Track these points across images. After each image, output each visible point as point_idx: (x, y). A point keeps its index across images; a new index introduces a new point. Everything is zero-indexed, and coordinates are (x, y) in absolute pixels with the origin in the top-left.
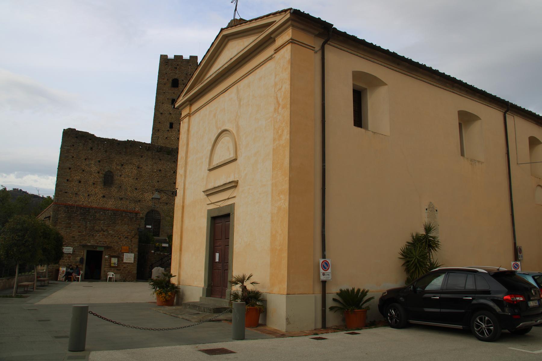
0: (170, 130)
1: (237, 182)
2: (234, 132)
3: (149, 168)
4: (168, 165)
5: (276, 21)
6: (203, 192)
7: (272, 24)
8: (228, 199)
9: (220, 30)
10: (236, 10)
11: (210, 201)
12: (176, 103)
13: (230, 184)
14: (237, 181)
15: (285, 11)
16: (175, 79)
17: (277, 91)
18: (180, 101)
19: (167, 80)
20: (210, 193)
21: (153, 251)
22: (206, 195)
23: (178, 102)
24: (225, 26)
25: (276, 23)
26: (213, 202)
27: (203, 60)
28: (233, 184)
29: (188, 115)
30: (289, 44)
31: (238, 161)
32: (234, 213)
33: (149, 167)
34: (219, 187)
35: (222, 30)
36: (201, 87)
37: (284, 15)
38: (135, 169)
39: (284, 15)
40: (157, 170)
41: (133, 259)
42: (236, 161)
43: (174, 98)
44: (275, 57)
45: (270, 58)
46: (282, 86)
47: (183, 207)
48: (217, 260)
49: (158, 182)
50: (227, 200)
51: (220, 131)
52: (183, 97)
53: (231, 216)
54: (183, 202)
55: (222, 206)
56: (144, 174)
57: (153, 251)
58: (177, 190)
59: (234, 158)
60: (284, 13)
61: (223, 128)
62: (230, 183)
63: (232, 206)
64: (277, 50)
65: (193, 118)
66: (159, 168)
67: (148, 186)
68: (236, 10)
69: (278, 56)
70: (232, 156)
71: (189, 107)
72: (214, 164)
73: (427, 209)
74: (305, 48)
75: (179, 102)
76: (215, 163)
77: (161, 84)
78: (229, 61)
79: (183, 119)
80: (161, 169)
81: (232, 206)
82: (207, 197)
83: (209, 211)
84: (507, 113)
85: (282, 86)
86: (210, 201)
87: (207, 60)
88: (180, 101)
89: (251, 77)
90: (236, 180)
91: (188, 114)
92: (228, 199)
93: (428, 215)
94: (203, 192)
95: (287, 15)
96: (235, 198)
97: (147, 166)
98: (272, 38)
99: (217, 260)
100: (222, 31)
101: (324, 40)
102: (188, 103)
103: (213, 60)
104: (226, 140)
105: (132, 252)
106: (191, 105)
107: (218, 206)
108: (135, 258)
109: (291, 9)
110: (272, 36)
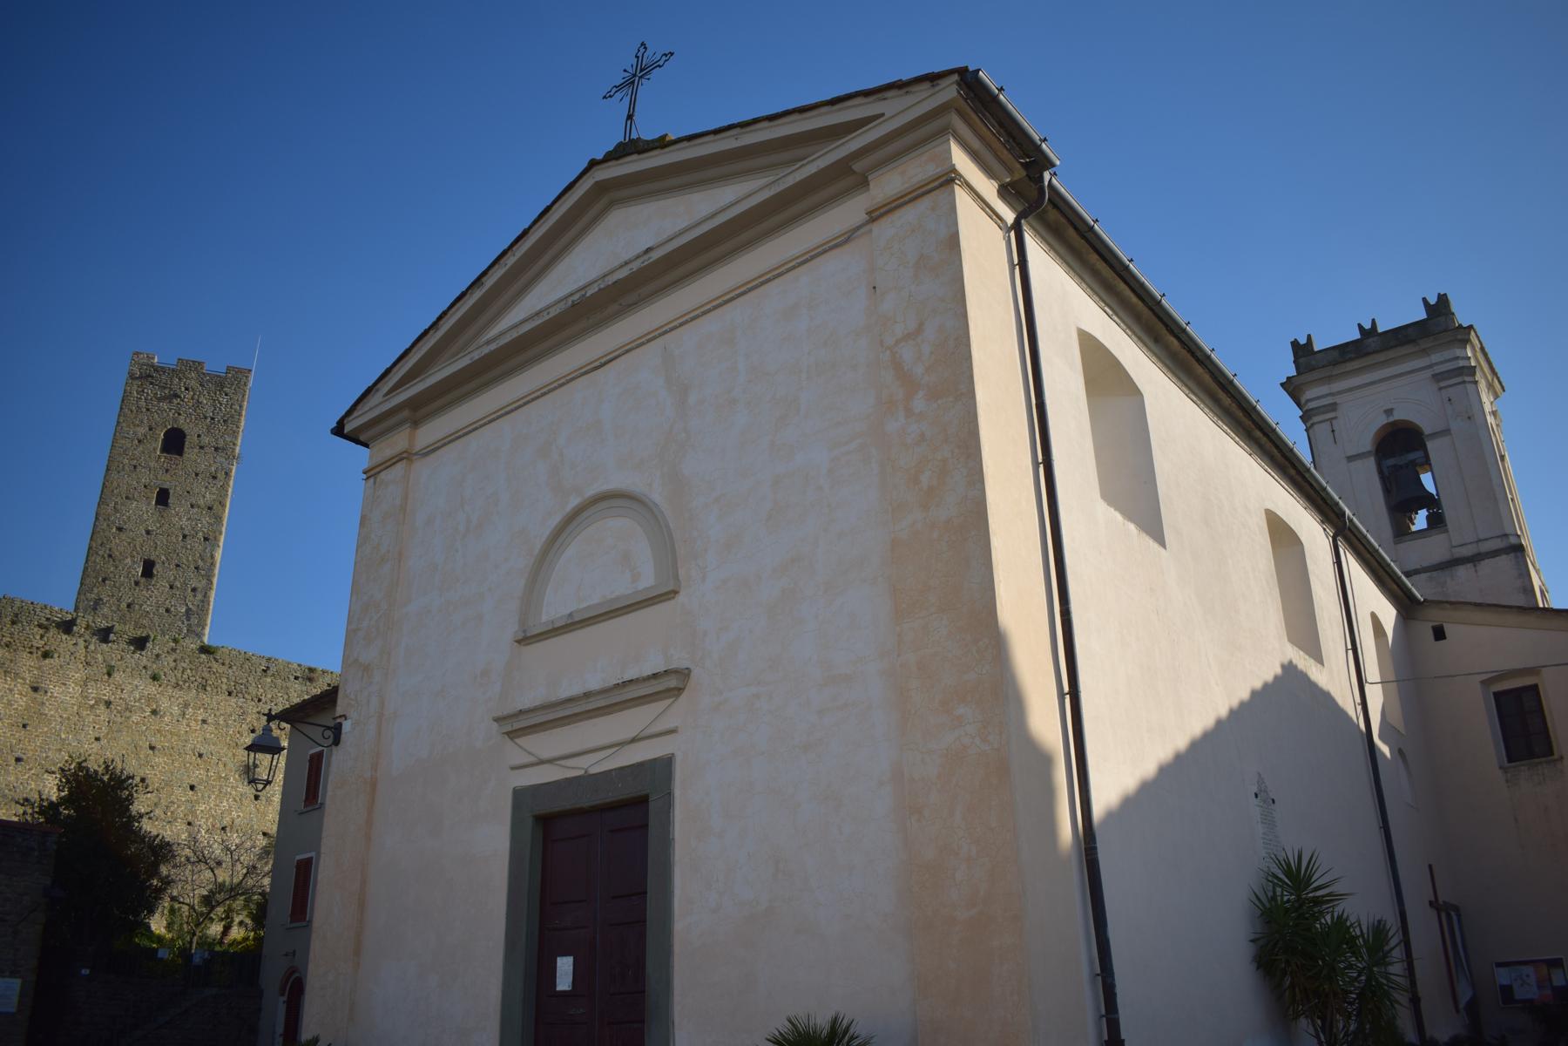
0: (143, 580)
1: (684, 674)
2: (657, 495)
3: (70, 693)
4: (137, 686)
5: (883, 115)
6: (497, 720)
7: (866, 125)
8: (633, 740)
9: (585, 165)
10: (630, 117)
11: (529, 753)
12: (351, 418)
13: (653, 682)
14: (686, 671)
15: (933, 78)
16: (173, 429)
17: (897, 342)
18: (371, 409)
19: (147, 429)
20: (518, 725)
21: (86, 972)
22: (508, 733)
23: (360, 413)
24: (600, 156)
25: (884, 121)
26: (545, 755)
27: (497, 266)
28: (672, 682)
29: (404, 455)
30: (943, 188)
31: (681, 598)
32: (669, 795)
33: (71, 690)
34: (570, 700)
35: (593, 164)
36: (486, 355)
37: (925, 94)
38: (21, 694)
39: (925, 94)
40: (96, 702)
41: (15, 999)
42: (673, 598)
43: (166, 487)
44: (871, 231)
45: (847, 238)
46: (921, 324)
47: (373, 785)
48: (564, 982)
49: (97, 739)
50: (626, 747)
51: (574, 502)
52: (384, 396)
53: (652, 806)
54: (1498, 537)
55: (594, 770)
56: (51, 710)
57: (86, 972)
58: (340, 725)
59: (671, 588)
60: (927, 85)
61: (591, 492)
62: (655, 676)
63: (662, 769)
64: (874, 216)
65: (422, 468)
66: (105, 695)
67: (60, 750)
68: (630, 117)
69: (886, 229)
70: (648, 580)
71: (408, 430)
72: (544, 618)
73: (1256, 796)
74: (614, 363)
75: (366, 412)
76: (555, 607)
77: (126, 437)
78: (638, 257)
79: (378, 470)
80: (112, 699)
81: (662, 769)
82: (512, 739)
83: (520, 796)
84: (1339, 538)
85: (921, 324)
86: (529, 753)
87: (512, 267)
88: (371, 409)
89: (735, 313)
90: (684, 664)
91: (405, 452)
92: (633, 740)
93: (1262, 815)
94: (497, 720)
95: (937, 92)
96: (673, 735)
97: (65, 684)
98: (854, 172)
99: (564, 982)
100: (595, 169)
101: (1020, 208)
102: (406, 413)
103: (541, 262)
104: (615, 527)
105: (13, 974)
106: (416, 424)
107: (581, 773)
108: (22, 994)
109: (962, 72)
110: (858, 166)
